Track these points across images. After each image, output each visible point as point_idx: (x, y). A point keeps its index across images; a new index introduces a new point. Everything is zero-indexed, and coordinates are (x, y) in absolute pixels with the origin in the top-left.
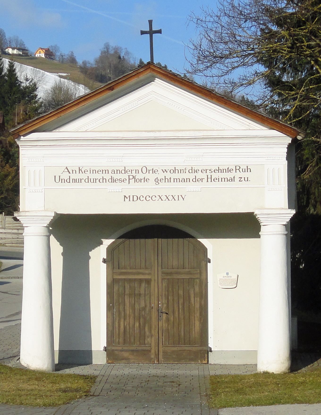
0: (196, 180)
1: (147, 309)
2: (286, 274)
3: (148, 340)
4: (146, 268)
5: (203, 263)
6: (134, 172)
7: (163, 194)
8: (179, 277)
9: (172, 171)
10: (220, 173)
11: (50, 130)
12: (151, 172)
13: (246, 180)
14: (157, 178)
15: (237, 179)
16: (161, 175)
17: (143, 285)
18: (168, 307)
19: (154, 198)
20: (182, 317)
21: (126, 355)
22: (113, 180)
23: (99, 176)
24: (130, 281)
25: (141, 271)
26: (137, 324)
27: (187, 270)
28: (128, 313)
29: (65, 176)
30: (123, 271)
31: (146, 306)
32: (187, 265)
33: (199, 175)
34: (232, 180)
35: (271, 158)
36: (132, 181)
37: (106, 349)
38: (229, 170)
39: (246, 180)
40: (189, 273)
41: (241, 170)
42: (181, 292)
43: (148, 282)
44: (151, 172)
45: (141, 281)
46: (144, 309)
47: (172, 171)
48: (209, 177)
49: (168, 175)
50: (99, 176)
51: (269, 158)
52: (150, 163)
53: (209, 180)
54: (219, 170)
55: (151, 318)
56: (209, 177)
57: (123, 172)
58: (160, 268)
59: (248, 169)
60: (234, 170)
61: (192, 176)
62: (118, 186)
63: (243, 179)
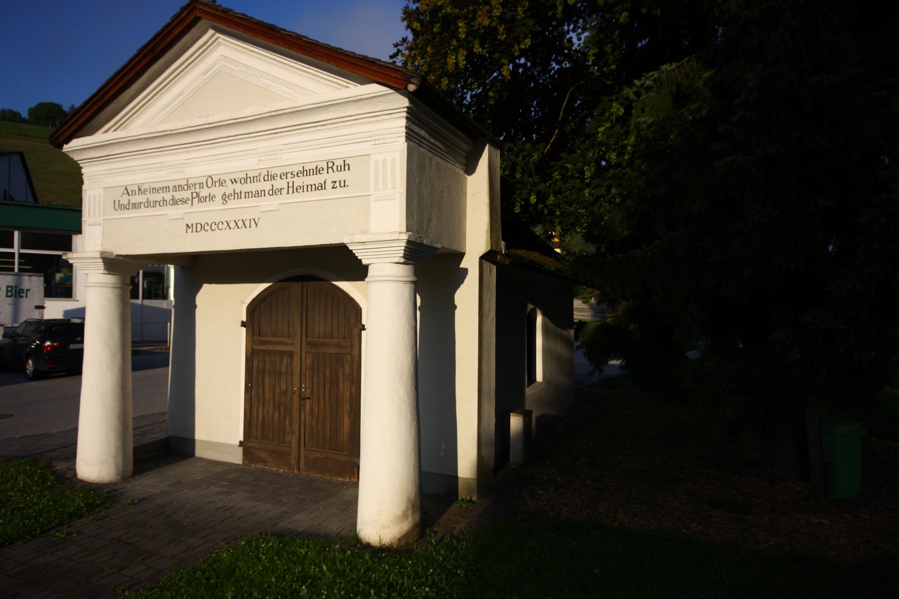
0: (274, 192)
1: (289, 394)
2: (119, 357)
3: (288, 438)
4: (289, 336)
5: (356, 331)
6: (198, 186)
7: (231, 218)
8: (327, 350)
9: (243, 181)
10: (305, 177)
11: (91, 133)
12: (217, 184)
13: (342, 185)
14: (225, 194)
15: (329, 185)
16: (229, 189)
17: (285, 360)
18: (312, 392)
19: (220, 226)
20: (328, 409)
21: (263, 455)
22: (175, 202)
23: (158, 197)
24: (271, 353)
25: (282, 339)
26: (277, 414)
27: (335, 341)
28: (267, 397)
29: (124, 200)
30: (265, 339)
31: (287, 389)
32: (335, 334)
33: (279, 183)
34: (322, 187)
35: (381, 141)
36: (196, 201)
37: (241, 444)
38: (318, 171)
39: (342, 185)
40: (338, 346)
41: (335, 168)
42: (328, 373)
43: (291, 355)
44: (217, 184)
45: (282, 353)
46: (285, 393)
47: (243, 181)
48: (291, 185)
49: (238, 187)
50: (158, 197)
51: (377, 142)
52: (217, 168)
53: (291, 189)
54: (304, 172)
55: (292, 407)
56: (291, 185)
57: (186, 188)
58: (304, 336)
59: (346, 166)
60: (325, 169)
61: (267, 186)
62: (173, 212)
63: (337, 184)
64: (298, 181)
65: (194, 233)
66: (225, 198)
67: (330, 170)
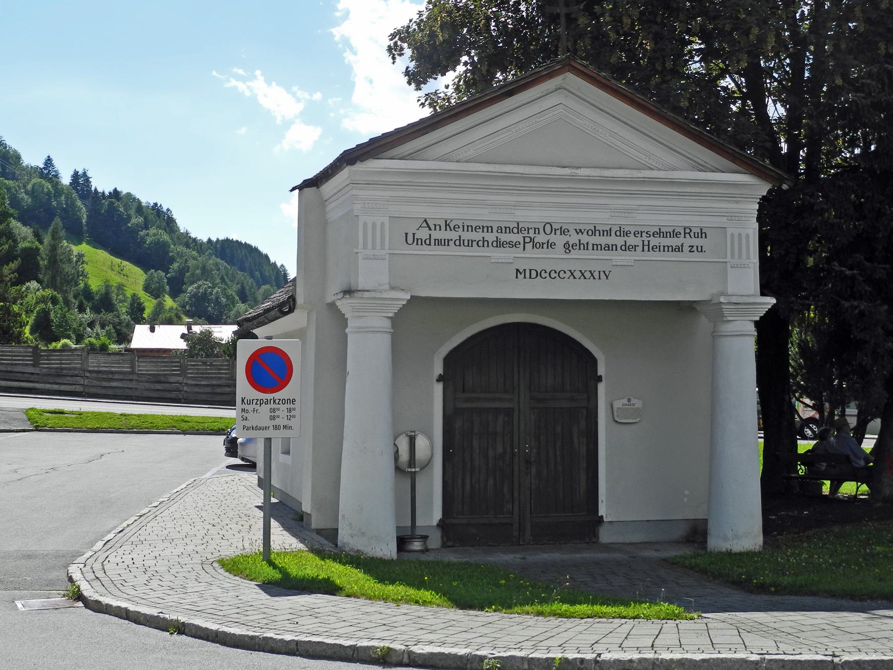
34: (679, 249)
41: (692, 234)
45: (497, 411)
54: (659, 233)
64: (654, 241)
65: (528, 279)
66: (567, 247)
67: (687, 235)
